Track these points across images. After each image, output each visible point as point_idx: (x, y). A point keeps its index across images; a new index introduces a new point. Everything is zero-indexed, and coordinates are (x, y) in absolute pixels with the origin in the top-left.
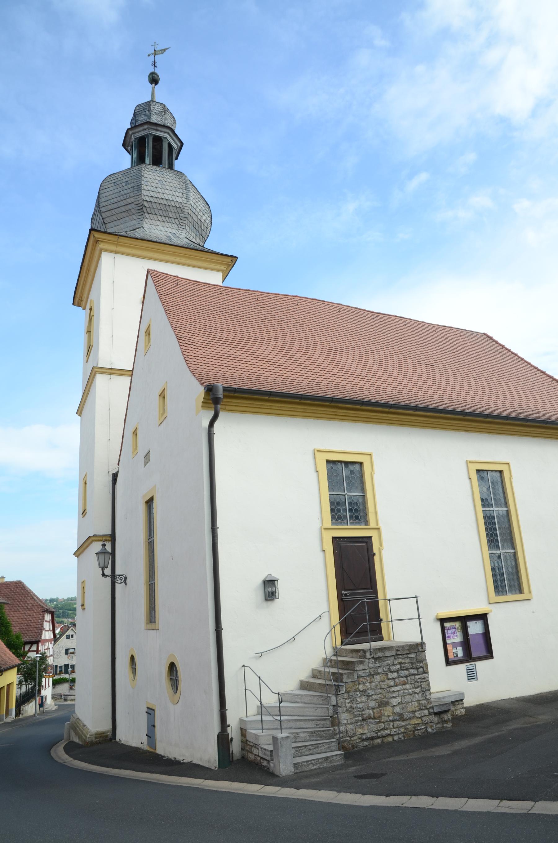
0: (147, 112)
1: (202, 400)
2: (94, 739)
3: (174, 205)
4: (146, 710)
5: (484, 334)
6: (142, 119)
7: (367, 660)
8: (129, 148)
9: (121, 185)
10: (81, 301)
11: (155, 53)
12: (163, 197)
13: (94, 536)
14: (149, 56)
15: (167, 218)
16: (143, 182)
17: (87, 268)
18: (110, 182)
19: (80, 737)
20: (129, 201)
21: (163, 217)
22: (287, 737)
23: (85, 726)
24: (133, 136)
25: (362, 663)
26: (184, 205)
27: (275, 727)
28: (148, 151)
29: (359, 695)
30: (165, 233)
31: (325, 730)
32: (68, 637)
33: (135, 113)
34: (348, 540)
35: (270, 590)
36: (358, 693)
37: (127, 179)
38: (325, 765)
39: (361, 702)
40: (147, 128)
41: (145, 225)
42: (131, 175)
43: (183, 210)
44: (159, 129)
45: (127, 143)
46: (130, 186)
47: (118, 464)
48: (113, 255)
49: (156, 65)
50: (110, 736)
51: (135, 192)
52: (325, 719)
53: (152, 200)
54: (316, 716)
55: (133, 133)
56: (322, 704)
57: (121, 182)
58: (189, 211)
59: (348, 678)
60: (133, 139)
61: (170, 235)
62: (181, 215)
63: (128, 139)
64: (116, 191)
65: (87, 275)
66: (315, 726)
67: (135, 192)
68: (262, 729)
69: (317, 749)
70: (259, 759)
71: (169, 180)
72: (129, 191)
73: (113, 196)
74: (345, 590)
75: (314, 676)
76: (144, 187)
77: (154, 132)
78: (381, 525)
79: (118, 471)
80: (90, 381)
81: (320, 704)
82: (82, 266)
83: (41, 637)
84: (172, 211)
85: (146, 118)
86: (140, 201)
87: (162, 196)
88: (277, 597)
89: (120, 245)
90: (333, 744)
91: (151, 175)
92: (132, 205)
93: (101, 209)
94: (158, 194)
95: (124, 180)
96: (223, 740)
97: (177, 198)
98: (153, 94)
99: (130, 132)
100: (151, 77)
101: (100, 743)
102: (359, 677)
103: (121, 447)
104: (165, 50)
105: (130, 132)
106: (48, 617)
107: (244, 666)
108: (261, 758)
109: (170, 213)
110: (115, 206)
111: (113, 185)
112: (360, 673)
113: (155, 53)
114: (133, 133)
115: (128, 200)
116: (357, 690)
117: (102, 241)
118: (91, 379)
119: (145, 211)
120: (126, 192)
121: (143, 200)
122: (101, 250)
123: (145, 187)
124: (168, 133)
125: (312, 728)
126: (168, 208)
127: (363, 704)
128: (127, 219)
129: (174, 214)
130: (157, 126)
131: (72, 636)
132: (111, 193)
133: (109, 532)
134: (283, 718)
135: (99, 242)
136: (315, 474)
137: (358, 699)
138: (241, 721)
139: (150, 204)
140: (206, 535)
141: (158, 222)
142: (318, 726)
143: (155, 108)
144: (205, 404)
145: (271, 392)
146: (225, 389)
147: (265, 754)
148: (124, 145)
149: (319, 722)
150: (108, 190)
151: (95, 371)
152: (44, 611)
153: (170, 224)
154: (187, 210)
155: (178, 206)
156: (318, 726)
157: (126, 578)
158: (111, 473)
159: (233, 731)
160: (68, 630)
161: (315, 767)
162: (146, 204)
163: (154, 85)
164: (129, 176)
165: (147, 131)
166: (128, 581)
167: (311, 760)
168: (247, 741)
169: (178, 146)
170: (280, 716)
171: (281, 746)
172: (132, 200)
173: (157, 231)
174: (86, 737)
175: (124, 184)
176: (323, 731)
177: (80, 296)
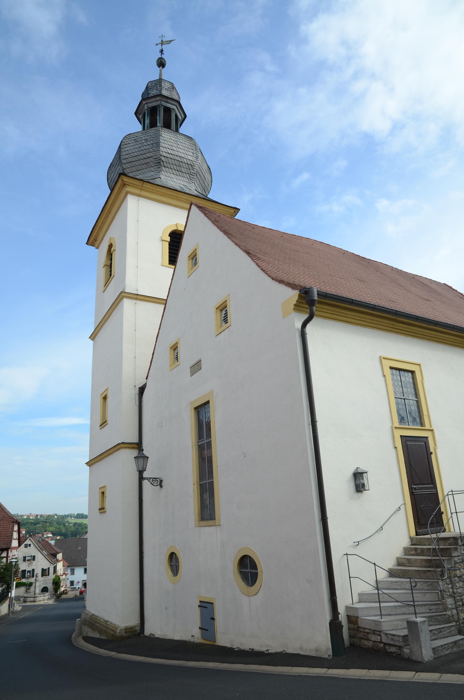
0: (159, 87)
1: (295, 302)
2: (124, 634)
3: (186, 162)
4: (199, 604)
5: (444, 284)
6: (154, 92)
7: (459, 547)
8: (141, 116)
9: (140, 142)
10: (96, 240)
11: (162, 43)
12: (178, 155)
13: (123, 443)
14: (157, 45)
15: (180, 172)
16: (161, 140)
17: (109, 210)
18: (130, 139)
19: (100, 632)
20: (148, 155)
21: (177, 172)
22: (424, 621)
23: (108, 621)
24: (146, 106)
25: (456, 549)
26: (194, 163)
27: (388, 613)
28: (160, 118)
29: (458, 580)
30: (179, 184)
31: (442, 615)
32: (26, 546)
33: (147, 87)
34: (412, 439)
35: (359, 481)
36: (456, 578)
37: (146, 137)
38: (455, 649)
39: (460, 588)
40: (159, 100)
41: (162, 177)
42: (150, 134)
43: (194, 167)
44: (170, 101)
45: (140, 112)
46: (149, 143)
47: (147, 379)
48: (137, 198)
49: (163, 52)
50: (138, 631)
51: (154, 148)
52: (438, 604)
53: (168, 155)
54: (425, 601)
55: (146, 103)
56: (427, 590)
57: (141, 139)
58: (198, 168)
59: (448, 564)
60: (146, 108)
61: (182, 186)
62: (192, 171)
63: (141, 108)
64: (136, 146)
65: (107, 216)
66: (429, 611)
67: (154, 148)
68: (381, 615)
69: (440, 634)
70: (382, 645)
71: (182, 141)
72: (148, 147)
73: (134, 151)
74: (414, 485)
75: (399, 564)
76: (162, 144)
77: (164, 104)
78: (433, 427)
79: (146, 383)
80: (114, 306)
81: (424, 590)
82: (104, 207)
83: (11, 544)
84: (185, 167)
85: (157, 92)
86: (158, 156)
87: (176, 153)
88: (367, 488)
89: (145, 190)
90: (453, 628)
91: (166, 137)
92: (151, 158)
93: (123, 161)
94: (173, 151)
95: (144, 138)
96: (335, 626)
97: (189, 156)
98: (160, 75)
99: (144, 102)
100: (159, 61)
101: (129, 637)
102: (456, 563)
103: (151, 362)
104: (171, 41)
105: (144, 102)
106: (16, 528)
107: (347, 554)
108: (385, 644)
109: (183, 169)
110: (136, 159)
111: (133, 141)
112: (456, 559)
113: (162, 43)
114: (146, 103)
115: (147, 154)
116: (455, 576)
117: (128, 185)
118: (115, 304)
119: (162, 165)
120: (145, 147)
121: (161, 155)
122: (127, 193)
123: (163, 145)
124: (176, 106)
125: (426, 613)
126: (181, 163)
127: (461, 589)
128: (146, 170)
129: (186, 170)
130: (167, 99)
131: (30, 545)
132: (131, 148)
133: (136, 440)
134: (382, 605)
135: (126, 186)
136: (383, 378)
137: (457, 585)
138: (347, 608)
139: (166, 159)
140: (306, 428)
141: (173, 175)
142: (432, 611)
143: (165, 85)
144: (298, 307)
145: (353, 300)
146: (320, 294)
147: (392, 639)
148: (136, 113)
149: (432, 607)
150: (128, 145)
151: (123, 295)
152: (13, 522)
153: (182, 178)
154: (196, 167)
155: (189, 163)
156: (432, 611)
157: (161, 481)
158: (137, 387)
159: (342, 617)
160: (26, 540)
161: (448, 652)
162: (163, 159)
163: (161, 68)
164: (148, 135)
165: (159, 102)
166: (163, 484)
167: (445, 645)
168: (359, 627)
169: (182, 117)
170: (414, 601)
171: (421, 631)
172: (151, 154)
173: (172, 182)
174: (115, 632)
175: (143, 141)
176: (440, 615)
177: (95, 236)
